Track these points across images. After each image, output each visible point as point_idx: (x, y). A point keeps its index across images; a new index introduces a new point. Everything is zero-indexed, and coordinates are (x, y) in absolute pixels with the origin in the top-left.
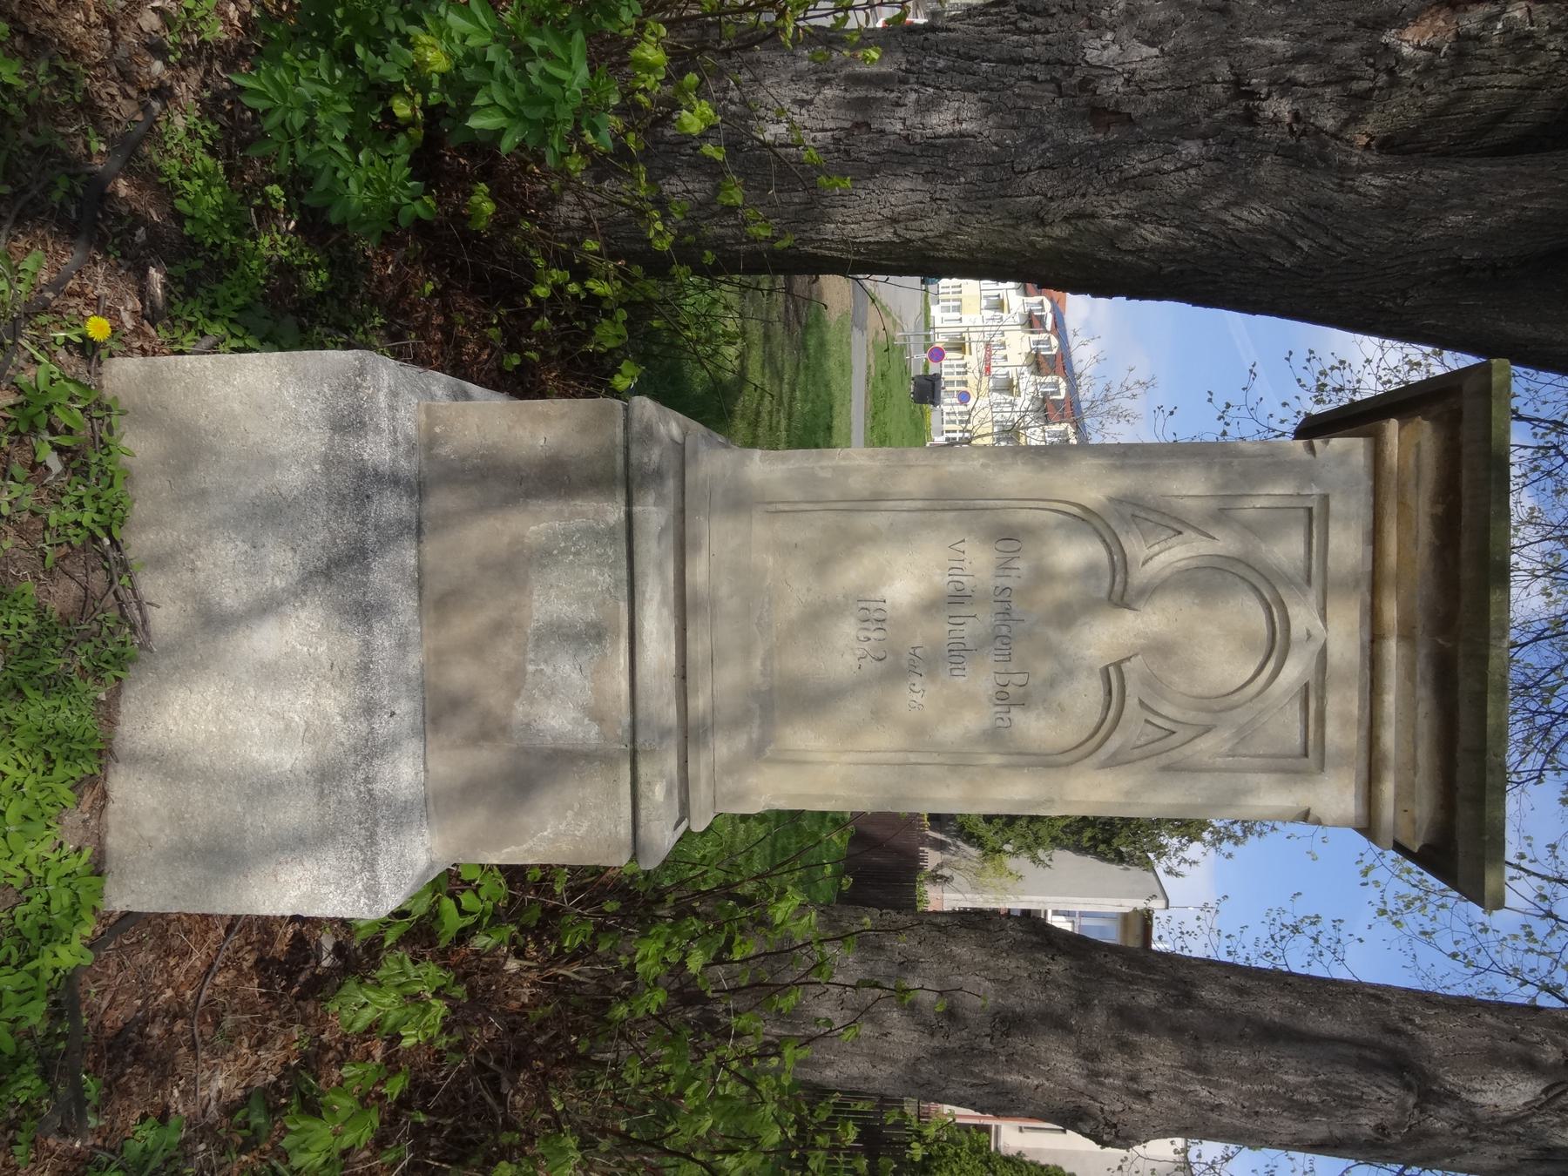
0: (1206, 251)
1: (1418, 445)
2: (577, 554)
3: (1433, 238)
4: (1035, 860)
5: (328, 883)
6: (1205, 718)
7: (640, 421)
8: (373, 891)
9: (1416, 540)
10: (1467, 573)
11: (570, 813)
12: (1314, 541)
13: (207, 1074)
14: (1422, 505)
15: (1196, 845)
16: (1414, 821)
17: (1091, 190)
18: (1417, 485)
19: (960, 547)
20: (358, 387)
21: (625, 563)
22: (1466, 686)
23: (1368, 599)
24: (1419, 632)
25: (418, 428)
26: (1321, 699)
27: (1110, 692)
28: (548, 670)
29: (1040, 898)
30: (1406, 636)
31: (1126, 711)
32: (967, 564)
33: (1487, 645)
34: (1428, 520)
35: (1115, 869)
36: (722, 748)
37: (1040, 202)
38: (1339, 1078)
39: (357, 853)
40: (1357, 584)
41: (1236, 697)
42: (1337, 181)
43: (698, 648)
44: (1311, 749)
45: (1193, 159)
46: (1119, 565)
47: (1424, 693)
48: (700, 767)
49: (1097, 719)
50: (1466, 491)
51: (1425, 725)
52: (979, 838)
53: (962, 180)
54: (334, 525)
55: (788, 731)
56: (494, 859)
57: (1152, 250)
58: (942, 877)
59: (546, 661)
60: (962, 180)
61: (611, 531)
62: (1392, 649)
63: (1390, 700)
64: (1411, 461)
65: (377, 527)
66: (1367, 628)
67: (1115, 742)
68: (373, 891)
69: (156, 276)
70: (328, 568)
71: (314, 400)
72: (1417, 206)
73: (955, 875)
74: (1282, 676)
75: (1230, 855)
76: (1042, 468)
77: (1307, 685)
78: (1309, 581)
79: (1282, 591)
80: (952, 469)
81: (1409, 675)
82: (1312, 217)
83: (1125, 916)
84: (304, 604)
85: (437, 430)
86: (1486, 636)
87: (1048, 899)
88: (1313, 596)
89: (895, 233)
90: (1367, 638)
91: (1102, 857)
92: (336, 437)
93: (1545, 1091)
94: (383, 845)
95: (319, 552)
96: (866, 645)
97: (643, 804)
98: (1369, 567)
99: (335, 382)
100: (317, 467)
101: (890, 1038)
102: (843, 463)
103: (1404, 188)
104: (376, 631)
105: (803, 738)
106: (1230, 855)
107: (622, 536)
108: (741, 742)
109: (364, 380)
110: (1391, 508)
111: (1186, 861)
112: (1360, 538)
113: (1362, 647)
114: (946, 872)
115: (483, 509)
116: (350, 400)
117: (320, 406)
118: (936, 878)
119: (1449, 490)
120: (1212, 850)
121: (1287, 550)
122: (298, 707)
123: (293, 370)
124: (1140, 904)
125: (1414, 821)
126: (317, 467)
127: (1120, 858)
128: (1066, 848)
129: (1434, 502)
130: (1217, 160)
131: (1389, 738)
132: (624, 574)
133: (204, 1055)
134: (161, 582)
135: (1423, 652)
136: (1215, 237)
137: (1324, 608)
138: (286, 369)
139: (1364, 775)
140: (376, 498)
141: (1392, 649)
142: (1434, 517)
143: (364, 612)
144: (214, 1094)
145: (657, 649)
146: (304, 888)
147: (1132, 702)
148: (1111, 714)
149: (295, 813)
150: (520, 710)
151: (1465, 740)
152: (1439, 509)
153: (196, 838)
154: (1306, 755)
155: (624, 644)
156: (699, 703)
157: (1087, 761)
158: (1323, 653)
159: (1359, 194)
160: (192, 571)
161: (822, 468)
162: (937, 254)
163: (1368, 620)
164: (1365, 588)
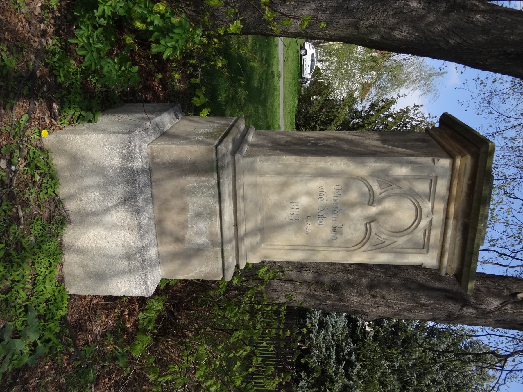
0: (417, 42)
1: (466, 164)
5: (133, 287)
7: (221, 154)
8: (147, 289)
9: (462, 192)
11: (204, 266)
13: (95, 328)
14: (465, 181)
16: (452, 268)
17: (376, 18)
18: (464, 176)
20: (129, 146)
21: (217, 195)
22: (470, 235)
24: (459, 218)
25: (148, 154)
26: (429, 234)
27: (367, 230)
28: (195, 227)
30: (456, 218)
31: (371, 236)
32: (324, 193)
36: (248, 242)
37: (357, 21)
38: (438, 302)
42: (467, 18)
43: (241, 215)
45: (415, 8)
46: (372, 195)
48: (243, 249)
49: (363, 238)
50: (477, 181)
51: (458, 242)
53: (328, 12)
54: (126, 188)
56: (181, 278)
57: (398, 40)
59: (194, 224)
60: (328, 12)
61: (213, 186)
62: (451, 222)
63: (450, 232)
64: (463, 168)
65: (139, 188)
70: (125, 201)
71: (115, 150)
72: (494, 31)
80: (321, 165)
81: (455, 229)
82: (456, 32)
84: (118, 211)
85: (154, 154)
90: (445, 217)
92: (124, 162)
93: (501, 304)
94: (149, 277)
95: (122, 196)
96: (293, 216)
99: (122, 145)
100: (118, 171)
101: (297, 291)
102: (286, 163)
103: (490, 24)
104: (142, 219)
109: (131, 144)
110: (455, 183)
112: (446, 189)
113: (443, 220)
115: (171, 177)
116: (127, 150)
117: (117, 152)
119: (473, 177)
122: (119, 240)
125: (452, 268)
126: (118, 171)
129: (469, 180)
130: (423, 9)
131: (448, 245)
133: (93, 323)
134: (71, 204)
135: (460, 223)
136: (421, 38)
139: (439, 255)
140: (138, 180)
141: (451, 222)
143: (137, 213)
144: (98, 333)
145: (228, 216)
146: (126, 289)
147: (373, 234)
148: (367, 237)
152: (470, 182)
155: (218, 219)
156: (242, 230)
158: (431, 221)
159: (474, 24)
160: (81, 201)
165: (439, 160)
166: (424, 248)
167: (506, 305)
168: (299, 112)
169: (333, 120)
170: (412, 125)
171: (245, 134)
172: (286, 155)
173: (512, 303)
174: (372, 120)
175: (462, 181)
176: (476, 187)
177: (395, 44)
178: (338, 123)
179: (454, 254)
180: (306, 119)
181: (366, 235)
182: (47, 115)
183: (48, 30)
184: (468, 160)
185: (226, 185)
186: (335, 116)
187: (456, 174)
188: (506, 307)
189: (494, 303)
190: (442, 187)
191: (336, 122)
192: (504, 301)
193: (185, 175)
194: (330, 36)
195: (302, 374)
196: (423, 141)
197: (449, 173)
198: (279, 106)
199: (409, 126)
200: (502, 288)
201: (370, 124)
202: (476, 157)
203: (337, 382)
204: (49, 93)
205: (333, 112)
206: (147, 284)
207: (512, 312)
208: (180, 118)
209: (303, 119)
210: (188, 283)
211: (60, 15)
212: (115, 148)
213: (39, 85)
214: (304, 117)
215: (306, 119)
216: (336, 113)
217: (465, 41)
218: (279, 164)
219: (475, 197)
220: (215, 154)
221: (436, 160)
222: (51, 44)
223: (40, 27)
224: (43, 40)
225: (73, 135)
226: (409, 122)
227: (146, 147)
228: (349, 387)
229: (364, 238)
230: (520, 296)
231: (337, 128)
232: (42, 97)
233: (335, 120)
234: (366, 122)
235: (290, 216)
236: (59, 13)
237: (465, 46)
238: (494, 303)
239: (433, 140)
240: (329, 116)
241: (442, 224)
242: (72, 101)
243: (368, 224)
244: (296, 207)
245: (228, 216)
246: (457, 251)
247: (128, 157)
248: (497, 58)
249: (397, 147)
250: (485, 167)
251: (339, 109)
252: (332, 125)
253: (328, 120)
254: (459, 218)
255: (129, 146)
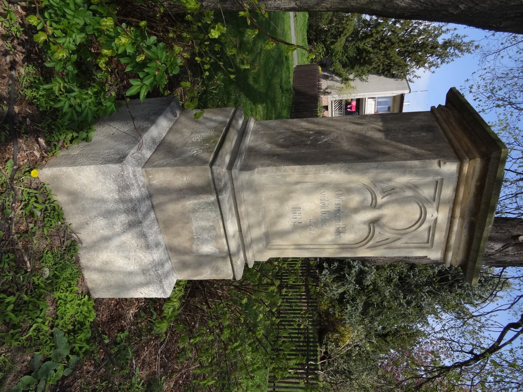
1: (475, 167)
2: (203, 209)
3: (515, 5)
4: (362, 80)
6: (398, 236)
7: (217, 173)
8: (164, 292)
9: (469, 193)
10: (483, 207)
12: (437, 190)
14: (473, 184)
15: (422, 69)
16: (456, 261)
18: (472, 178)
19: (324, 193)
22: (476, 234)
23: (452, 206)
29: (364, 94)
30: (462, 217)
31: (375, 236)
33: (484, 227)
34: (474, 186)
35: (392, 80)
39: (158, 285)
40: (449, 202)
41: (408, 230)
43: (244, 227)
44: (430, 240)
47: (465, 232)
49: (366, 235)
50: (487, 185)
51: (464, 238)
52: (341, 74)
55: (274, 241)
58: (327, 92)
62: (457, 222)
63: (456, 228)
64: (472, 171)
66: (451, 214)
67: (371, 243)
68: (164, 292)
69: (41, 140)
71: (110, 179)
73: (332, 91)
74: (423, 226)
75: (434, 72)
76: (350, 174)
77: (430, 227)
78: (434, 200)
79: (425, 205)
81: (461, 226)
83: (394, 97)
86: (485, 224)
87: (366, 94)
88: (435, 205)
89: (296, 4)
90: (450, 216)
91: (386, 76)
93: (502, 247)
94: (164, 283)
97: (235, 266)
98: (453, 198)
105: (278, 242)
106: (434, 72)
107: (217, 203)
108: (261, 246)
109: (124, 172)
111: (416, 76)
113: (448, 218)
114: (329, 90)
115: (171, 201)
118: (326, 93)
120: (428, 70)
121: (427, 192)
123: (100, 171)
124: (400, 92)
125: (456, 261)
127: (393, 76)
128: (374, 74)
129: (477, 181)
132: (219, 213)
135: (466, 221)
136: (427, 4)
137: (438, 208)
138: (97, 171)
141: (457, 222)
142: (476, 186)
145: (232, 228)
148: (371, 235)
149: (140, 279)
150: (195, 247)
151: (474, 247)
152: (479, 184)
153: (112, 283)
154: (428, 243)
157: (363, 247)
161: (277, 175)
162: (313, 10)
163: (451, 211)
164: (451, 203)
165: (445, 163)
166: (428, 243)
167: (508, 247)
168: (310, 26)
169: (342, 32)
170: (419, 30)
171: (246, 123)
172: (285, 165)
173: (514, 245)
174: (379, 29)
175: (470, 183)
176: (485, 190)
177: (398, 12)
178: (348, 35)
179: (459, 249)
180: (317, 34)
181: (370, 233)
182: (36, 148)
183: (17, 59)
184: (478, 163)
185: (226, 201)
186: (344, 29)
187: (464, 179)
188: (507, 249)
189: (496, 246)
190: (448, 192)
191: (346, 34)
192: (505, 244)
193: (184, 197)
194: (327, 8)
195: (324, 264)
196: (429, 129)
197: (455, 179)
198: (290, 27)
199: (417, 31)
200: (504, 232)
201: (378, 32)
202: (486, 159)
203: (354, 267)
204: (34, 124)
205: (343, 24)
206: (163, 288)
207: (513, 253)
208: (178, 115)
209: (314, 33)
210: (201, 282)
211: (27, 38)
212: (109, 177)
213: (19, 121)
214: (315, 31)
215: (317, 34)
216: (344, 25)
217: (477, 5)
218: (277, 175)
219: (483, 200)
220: (210, 172)
221: (442, 163)
222: (23, 73)
223: (6, 61)
224: (13, 73)
225: (65, 168)
226: (416, 27)
227: (141, 171)
228: (364, 272)
229: (368, 236)
230: (521, 238)
231: (346, 39)
232: (26, 133)
233: (344, 33)
234: (374, 31)
235: (293, 220)
236: (26, 35)
237: (477, 10)
238: (496, 246)
239: (439, 127)
240: (339, 28)
241: (448, 222)
242: (60, 126)
243: (371, 225)
244: (299, 212)
245: (232, 228)
246: (462, 246)
247: (124, 187)
248: (512, 20)
249: (400, 142)
250: (495, 176)
251: (347, 21)
252: (342, 37)
253: (338, 32)
254: (465, 217)
255: (123, 175)
